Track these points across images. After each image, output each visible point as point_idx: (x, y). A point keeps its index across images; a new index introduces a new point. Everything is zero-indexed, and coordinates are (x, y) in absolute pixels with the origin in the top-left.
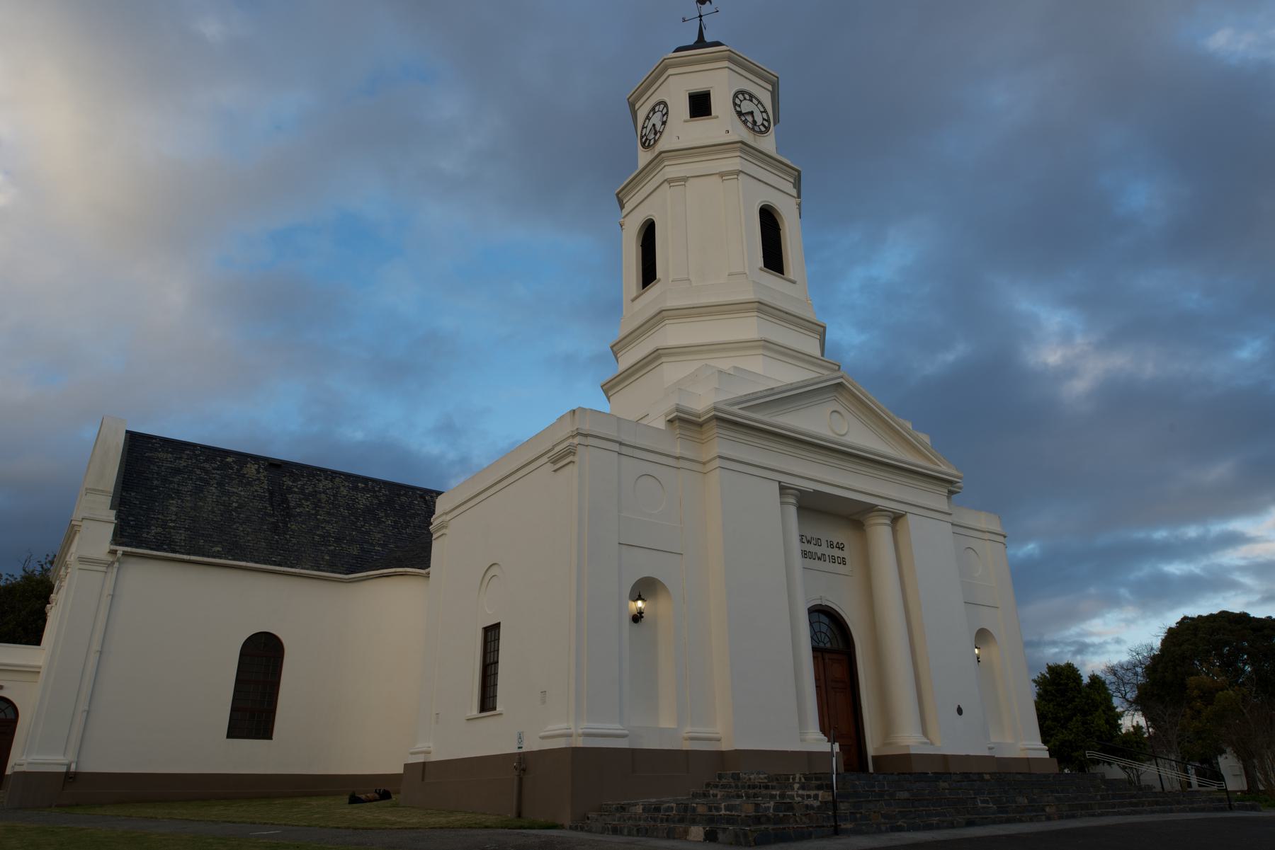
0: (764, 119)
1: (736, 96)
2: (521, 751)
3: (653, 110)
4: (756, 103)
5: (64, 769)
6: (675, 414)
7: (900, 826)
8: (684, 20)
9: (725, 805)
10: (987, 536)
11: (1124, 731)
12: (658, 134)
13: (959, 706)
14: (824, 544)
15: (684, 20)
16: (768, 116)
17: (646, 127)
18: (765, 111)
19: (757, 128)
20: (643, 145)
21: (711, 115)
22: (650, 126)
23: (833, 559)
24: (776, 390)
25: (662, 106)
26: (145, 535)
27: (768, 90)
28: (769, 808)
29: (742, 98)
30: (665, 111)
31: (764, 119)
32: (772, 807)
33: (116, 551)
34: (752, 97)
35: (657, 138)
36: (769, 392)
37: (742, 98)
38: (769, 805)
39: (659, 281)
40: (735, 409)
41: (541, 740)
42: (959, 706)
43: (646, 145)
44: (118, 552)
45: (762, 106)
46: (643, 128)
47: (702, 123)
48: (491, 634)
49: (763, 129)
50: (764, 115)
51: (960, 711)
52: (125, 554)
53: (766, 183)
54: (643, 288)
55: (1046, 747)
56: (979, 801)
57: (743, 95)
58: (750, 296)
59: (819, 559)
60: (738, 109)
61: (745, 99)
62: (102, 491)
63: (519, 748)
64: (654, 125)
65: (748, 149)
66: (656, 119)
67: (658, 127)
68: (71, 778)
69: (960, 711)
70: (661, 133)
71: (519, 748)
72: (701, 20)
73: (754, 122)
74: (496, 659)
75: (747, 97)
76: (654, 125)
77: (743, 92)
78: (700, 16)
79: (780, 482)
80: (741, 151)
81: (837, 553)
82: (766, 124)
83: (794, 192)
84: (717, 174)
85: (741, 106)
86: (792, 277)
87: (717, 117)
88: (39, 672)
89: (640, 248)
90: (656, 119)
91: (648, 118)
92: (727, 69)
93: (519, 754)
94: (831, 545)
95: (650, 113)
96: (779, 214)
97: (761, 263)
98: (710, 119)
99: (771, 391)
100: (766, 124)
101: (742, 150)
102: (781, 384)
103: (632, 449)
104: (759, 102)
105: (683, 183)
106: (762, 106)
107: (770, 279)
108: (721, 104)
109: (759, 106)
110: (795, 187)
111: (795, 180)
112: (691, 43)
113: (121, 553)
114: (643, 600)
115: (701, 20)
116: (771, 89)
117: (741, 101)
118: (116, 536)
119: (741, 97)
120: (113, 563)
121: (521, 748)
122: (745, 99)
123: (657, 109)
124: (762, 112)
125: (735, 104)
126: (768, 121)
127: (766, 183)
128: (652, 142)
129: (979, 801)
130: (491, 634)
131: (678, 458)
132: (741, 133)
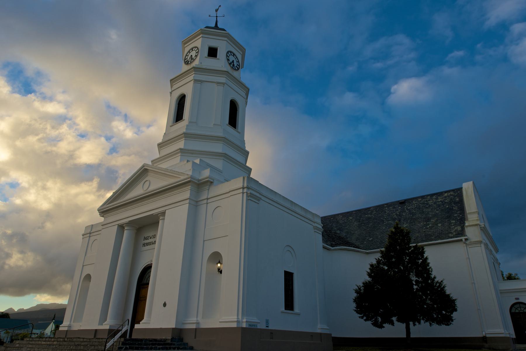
0: (237, 65)
1: (228, 52)
2: (267, 328)
3: (192, 49)
4: (235, 57)
6: (190, 179)
8: (210, 16)
9: (127, 347)
11: (416, 322)
12: (193, 60)
13: (165, 302)
15: (210, 16)
16: (239, 64)
17: (188, 56)
18: (238, 62)
19: (234, 68)
20: (185, 62)
21: (217, 57)
22: (190, 56)
25: (196, 49)
27: (241, 54)
29: (230, 54)
30: (197, 51)
31: (237, 65)
33: (462, 239)
34: (234, 55)
35: (192, 61)
37: (230, 54)
39: (184, 120)
42: (165, 302)
43: (187, 63)
44: (463, 240)
45: (238, 59)
46: (186, 55)
47: (212, 60)
48: (289, 277)
49: (237, 69)
50: (238, 63)
51: (165, 305)
53: (181, 86)
54: (176, 122)
57: (231, 53)
58: (221, 134)
60: (228, 58)
61: (231, 55)
63: (267, 327)
64: (191, 56)
65: (229, 75)
66: (193, 53)
67: (193, 57)
69: (165, 305)
70: (194, 60)
71: (267, 327)
72: (217, 18)
73: (234, 65)
74: (148, 282)
75: (232, 54)
76: (191, 56)
77: (231, 52)
78: (217, 17)
80: (195, 71)
82: (238, 67)
83: (245, 97)
84: (215, 82)
85: (229, 57)
86: (239, 130)
87: (218, 59)
89: (177, 105)
90: (193, 53)
91: (189, 52)
92: (226, 41)
95: (190, 50)
96: (238, 104)
97: (228, 123)
100: (238, 67)
101: (195, 71)
104: (237, 58)
105: (200, 83)
106: (238, 59)
107: (230, 129)
108: (221, 53)
109: (236, 59)
110: (246, 95)
111: (247, 92)
113: (464, 240)
115: (217, 18)
116: (242, 54)
117: (230, 55)
119: (230, 53)
121: (268, 327)
122: (231, 55)
123: (194, 49)
124: (237, 62)
125: (227, 56)
126: (239, 66)
127: (181, 86)
128: (189, 62)
130: (289, 277)
132: (228, 68)
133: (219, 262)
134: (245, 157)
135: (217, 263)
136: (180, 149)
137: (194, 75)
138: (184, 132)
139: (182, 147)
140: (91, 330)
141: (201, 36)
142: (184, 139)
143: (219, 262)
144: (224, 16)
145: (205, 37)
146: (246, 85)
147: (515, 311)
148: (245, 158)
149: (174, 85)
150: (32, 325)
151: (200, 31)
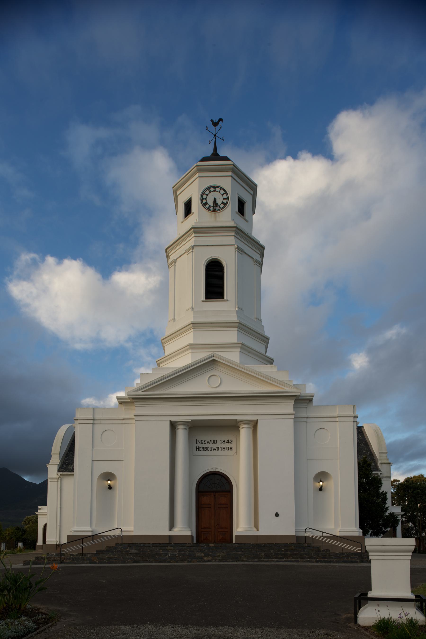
5: (55, 543)
7: (95, 562)
10: (338, 419)
14: (219, 442)
23: (224, 449)
24: (165, 377)
26: (69, 467)
27: (251, 194)
28: (53, 555)
32: (54, 555)
33: (378, 473)
36: (162, 378)
38: (53, 554)
40: (140, 392)
41: (70, 532)
44: (379, 474)
52: (61, 475)
55: (362, 531)
56: (169, 554)
59: (214, 450)
62: (56, 454)
68: (58, 546)
79: (170, 421)
80: (195, 233)
81: (227, 445)
88: (46, 514)
93: (170, 536)
94: (224, 442)
98: (240, 195)
99: (163, 378)
101: (195, 232)
102: (175, 370)
103: (100, 420)
110: (260, 257)
111: (261, 253)
112: (209, 155)
113: (380, 474)
114: (111, 481)
118: (60, 469)
120: (59, 478)
129: (169, 554)
131: (123, 419)
133: (109, 479)
134: (265, 344)
135: (319, 482)
136: (190, 345)
137: (194, 239)
138: (191, 321)
139: (192, 342)
140: (160, 535)
141: (197, 175)
142: (192, 330)
143: (109, 479)
144: (223, 140)
145: (249, 336)
146: (260, 242)
147: (215, 470)
148: (265, 346)
149: (170, 255)
150: (120, 530)
151: (196, 167)
